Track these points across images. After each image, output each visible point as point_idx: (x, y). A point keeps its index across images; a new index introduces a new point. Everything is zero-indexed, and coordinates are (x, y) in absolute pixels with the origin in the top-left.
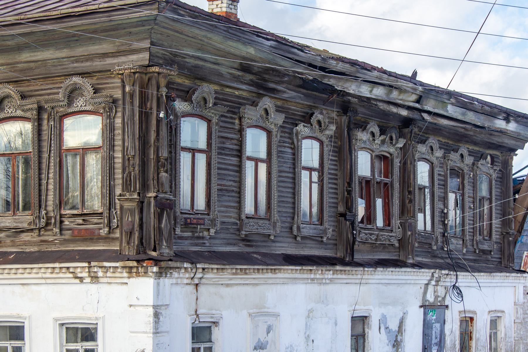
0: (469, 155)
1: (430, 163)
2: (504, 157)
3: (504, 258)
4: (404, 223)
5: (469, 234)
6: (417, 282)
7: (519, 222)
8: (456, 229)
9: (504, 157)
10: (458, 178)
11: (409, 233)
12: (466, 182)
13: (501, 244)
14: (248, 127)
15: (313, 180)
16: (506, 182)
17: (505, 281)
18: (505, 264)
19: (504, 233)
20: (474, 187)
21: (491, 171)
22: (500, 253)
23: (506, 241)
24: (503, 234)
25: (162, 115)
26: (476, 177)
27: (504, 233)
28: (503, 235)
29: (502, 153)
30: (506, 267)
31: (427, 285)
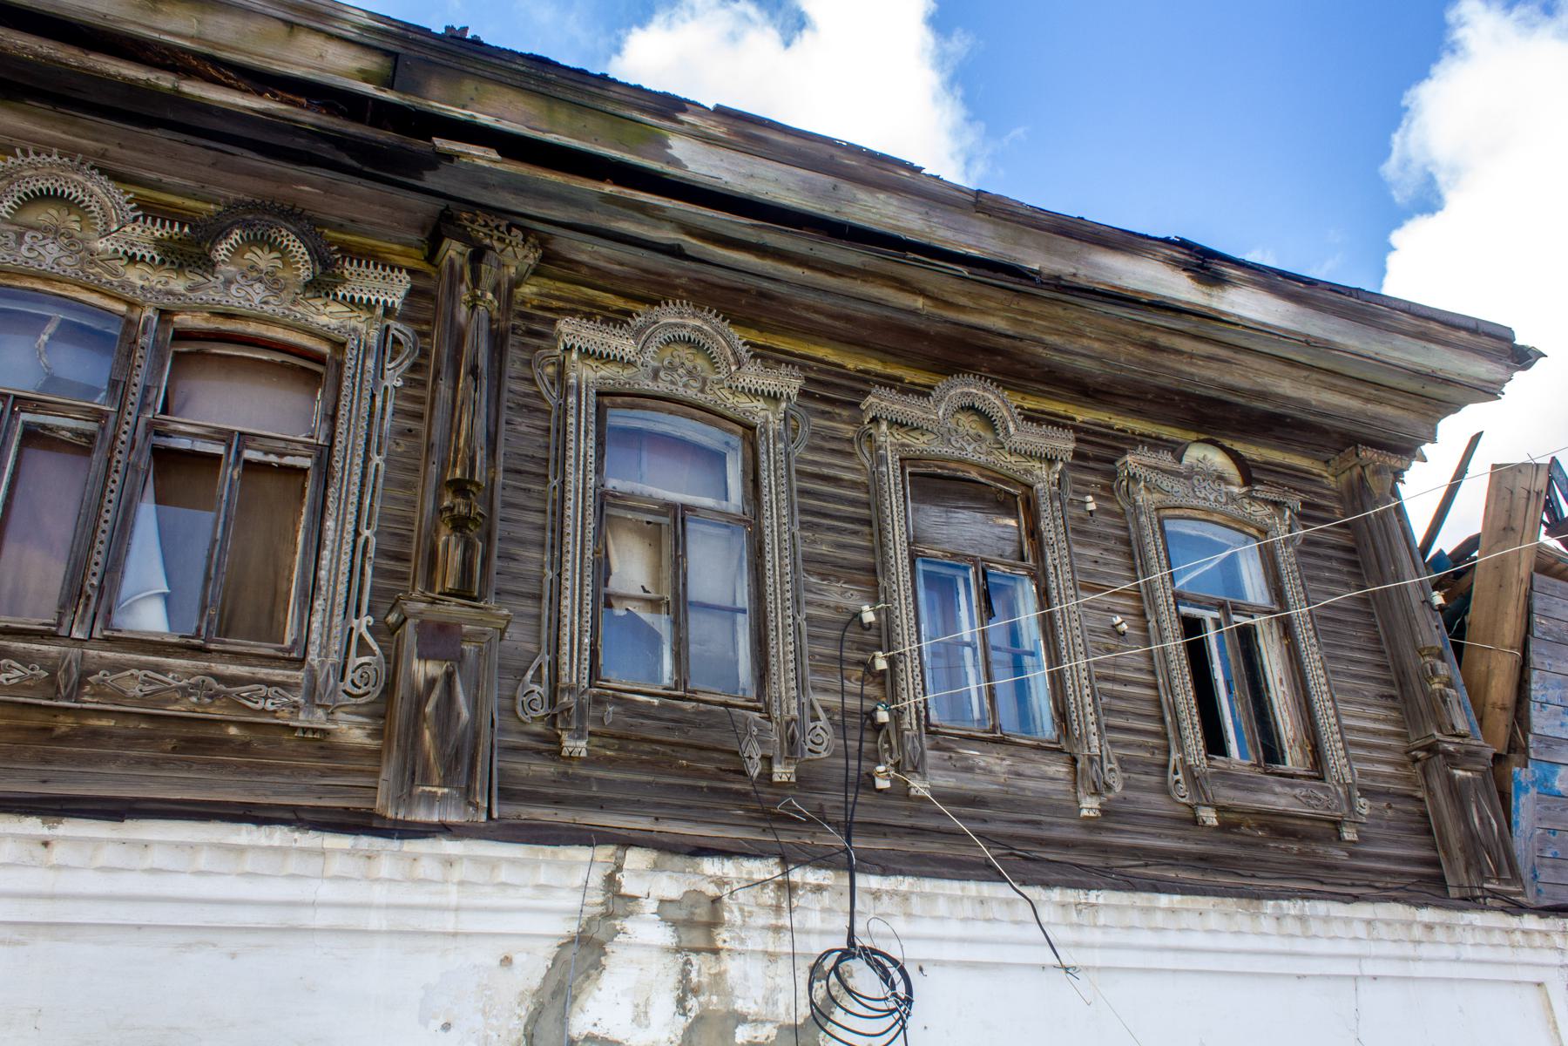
0: (754, 356)
1: (739, 429)
2: (1344, 478)
3: (1450, 861)
4: (393, 629)
5: (818, 649)
6: (469, 923)
7: (1503, 708)
8: (925, 695)
9: (1344, 478)
10: (1011, 511)
11: (423, 670)
12: (1046, 525)
13: (1421, 800)
14: (606, 585)
15: (1453, 956)
16: (1374, 559)
17: (1425, 950)
18: (1460, 886)
19: (1421, 754)
20: (1131, 556)
21: (1260, 512)
22: (1424, 839)
23: (1437, 784)
24: (1416, 760)
25: (233, 731)
26: (1137, 520)
27: (1421, 754)
28: (1418, 765)
29: (1327, 462)
30: (1465, 899)
31: (848, 1011)
